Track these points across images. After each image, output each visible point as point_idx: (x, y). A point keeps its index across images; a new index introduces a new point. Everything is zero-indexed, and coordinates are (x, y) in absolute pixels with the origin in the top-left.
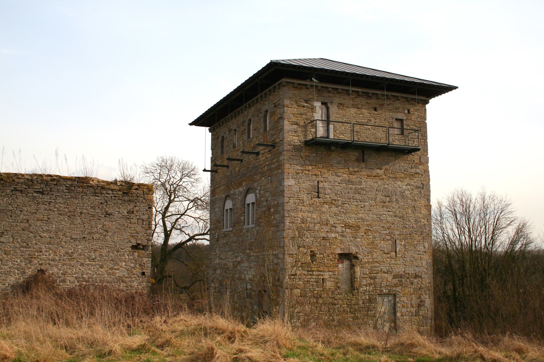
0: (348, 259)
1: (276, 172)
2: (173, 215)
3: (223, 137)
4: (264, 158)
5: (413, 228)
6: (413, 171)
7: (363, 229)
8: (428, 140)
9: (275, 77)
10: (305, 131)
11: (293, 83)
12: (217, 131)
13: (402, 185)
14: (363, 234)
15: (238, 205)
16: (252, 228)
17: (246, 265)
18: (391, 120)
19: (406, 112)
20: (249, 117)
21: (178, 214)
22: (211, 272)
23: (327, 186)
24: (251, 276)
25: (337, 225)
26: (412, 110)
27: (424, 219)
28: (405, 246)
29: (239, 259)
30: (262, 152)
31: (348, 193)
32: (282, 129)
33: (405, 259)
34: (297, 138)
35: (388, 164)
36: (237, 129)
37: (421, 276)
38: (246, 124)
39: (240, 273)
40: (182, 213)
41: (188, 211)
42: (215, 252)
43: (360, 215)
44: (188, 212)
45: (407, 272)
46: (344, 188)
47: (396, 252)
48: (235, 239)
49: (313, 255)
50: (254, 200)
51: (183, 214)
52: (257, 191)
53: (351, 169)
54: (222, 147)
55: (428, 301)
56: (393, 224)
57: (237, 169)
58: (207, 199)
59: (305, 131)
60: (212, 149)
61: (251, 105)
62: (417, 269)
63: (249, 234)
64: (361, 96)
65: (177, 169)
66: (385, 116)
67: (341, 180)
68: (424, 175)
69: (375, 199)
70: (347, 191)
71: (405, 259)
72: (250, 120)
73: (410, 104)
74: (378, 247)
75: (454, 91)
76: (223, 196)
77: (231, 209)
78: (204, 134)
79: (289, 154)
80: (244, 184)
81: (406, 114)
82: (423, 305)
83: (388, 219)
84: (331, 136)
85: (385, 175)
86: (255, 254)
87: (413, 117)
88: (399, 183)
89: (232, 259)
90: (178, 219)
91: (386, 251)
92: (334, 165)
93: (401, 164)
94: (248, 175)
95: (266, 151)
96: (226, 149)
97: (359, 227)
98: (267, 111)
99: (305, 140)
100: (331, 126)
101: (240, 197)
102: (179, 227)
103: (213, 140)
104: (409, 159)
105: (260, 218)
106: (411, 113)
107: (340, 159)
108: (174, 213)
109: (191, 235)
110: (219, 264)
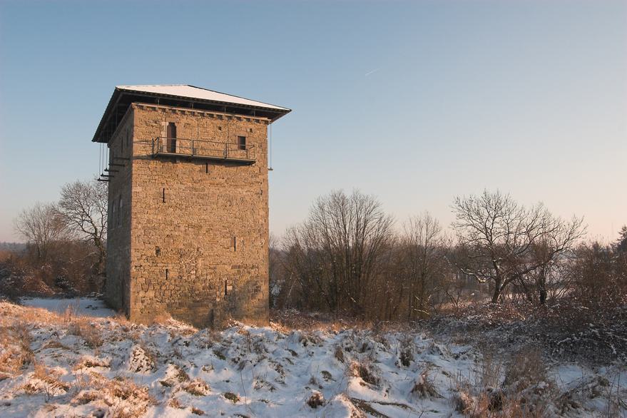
6: (253, 180)
88: (240, 190)
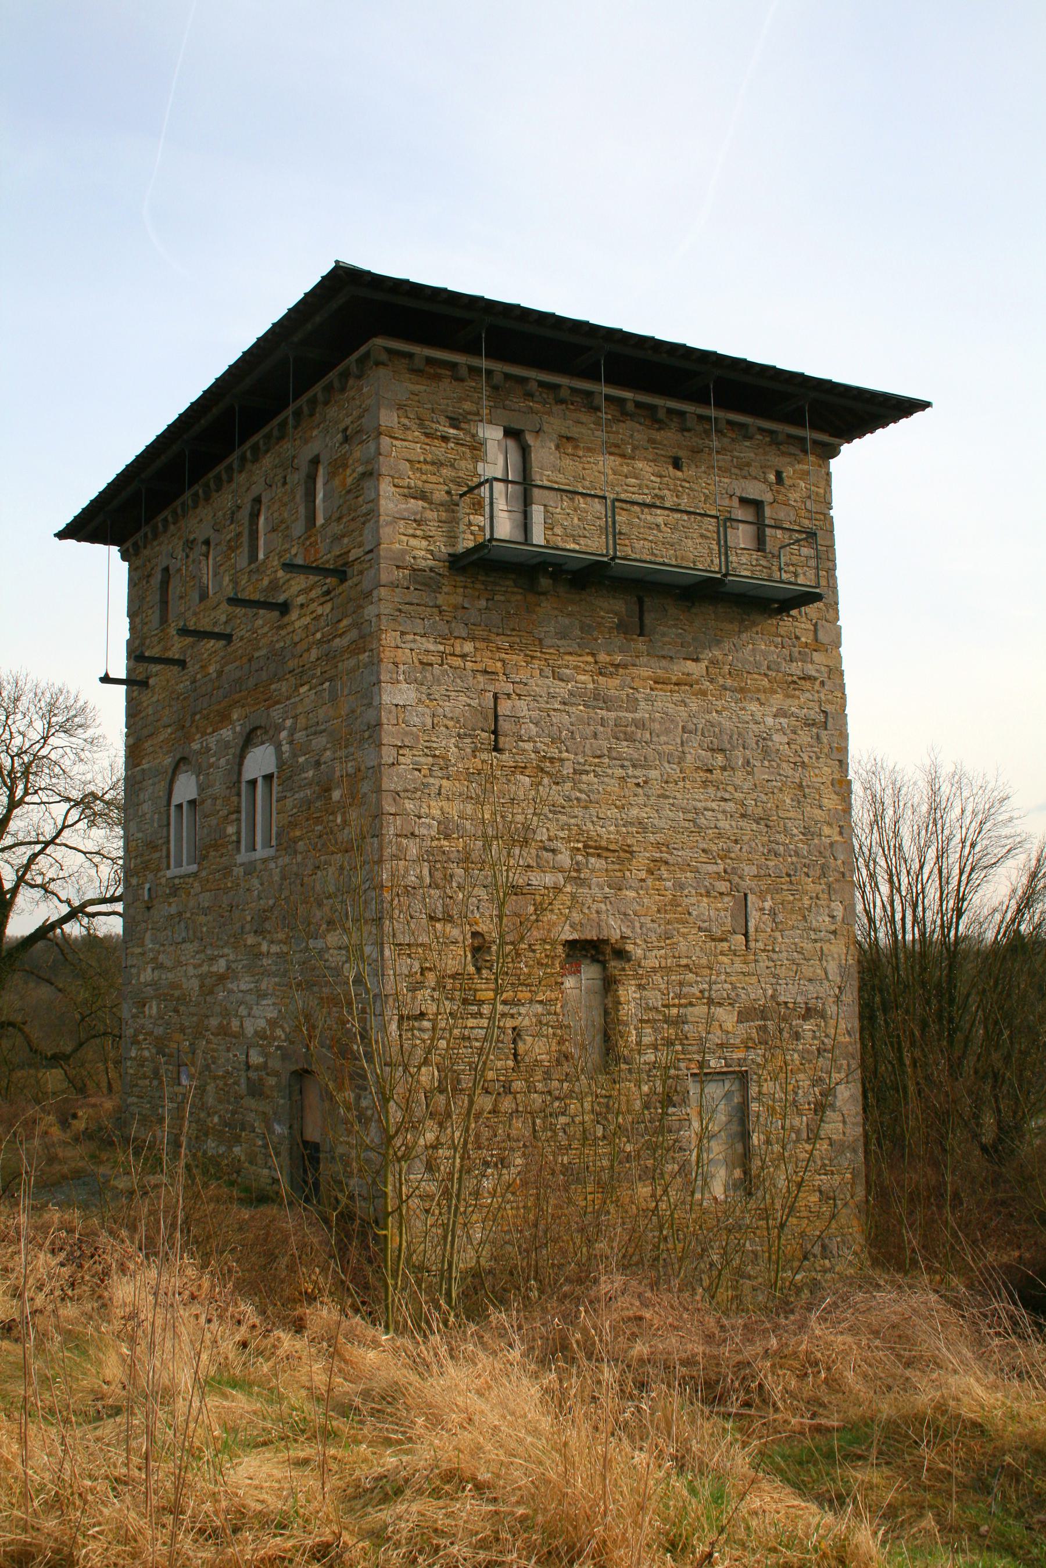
0: (595, 960)
1: (352, 662)
2: (22, 844)
3: (166, 570)
4: (307, 620)
5: (797, 854)
6: (796, 668)
7: (642, 859)
8: (838, 573)
9: (356, 322)
10: (451, 523)
11: (410, 356)
12: (146, 552)
13: (762, 715)
14: (643, 875)
15: (218, 788)
16: (265, 861)
17: (243, 987)
18: (726, 502)
19: (772, 477)
20: (255, 491)
21: (38, 842)
22: (126, 1011)
23: (525, 712)
24: (262, 1023)
25: (558, 845)
26: (788, 472)
27: (829, 824)
28: (773, 913)
29: (221, 966)
30: (301, 599)
31: (595, 736)
32: (372, 513)
33: (775, 956)
34: (424, 543)
35: (718, 643)
36: (214, 537)
37: (824, 1010)
38: (244, 515)
39: (226, 1014)
40: (48, 838)
41: (66, 833)
42: (143, 945)
43: (634, 812)
44: (66, 836)
45: (781, 999)
46: (580, 720)
47: (746, 934)
48: (206, 899)
49: (479, 948)
50: (271, 768)
51: (52, 841)
52: (284, 734)
53: (603, 657)
54: (164, 603)
55: (847, 1095)
56: (736, 842)
57: (211, 669)
58: (119, 794)
59: (451, 523)
60: (133, 614)
61: (263, 448)
62: (812, 989)
63: (256, 882)
64: (631, 416)
65: (32, 709)
66: (713, 485)
67: (571, 694)
68: (828, 683)
69: (681, 759)
70: (589, 731)
71: (775, 956)
72: (258, 500)
73: (783, 454)
74: (691, 919)
75: (918, 416)
76: (168, 761)
77: (192, 803)
78: (106, 567)
79: (398, 595)
80: (235, 717)
81: (770, 485)
82: (832, 1106)
83: (721, 824)
84: (538, 537)
85: (711, 681)
86: (275, 949)
87: (794, 496)
88: (753, 707)
89: (196, 967)
90: (35, 855)
91: (717, 932)
92: (548, 642)
93: (758, 646)
94: (251, 682)
95: (313, 594)
96: (175, 607)
97: (631, 853)
98: (315, 461)
99: (451, 551)
100: (537, 512)
101: (223, 761)
102: (39, 880)
103: (133, 583)
104: (782, 631)
105: (292, 825)
106: (787, 482)
107: (567, 621)
108: (21, 837)
109: (76, 903)
110: (153, 984)
